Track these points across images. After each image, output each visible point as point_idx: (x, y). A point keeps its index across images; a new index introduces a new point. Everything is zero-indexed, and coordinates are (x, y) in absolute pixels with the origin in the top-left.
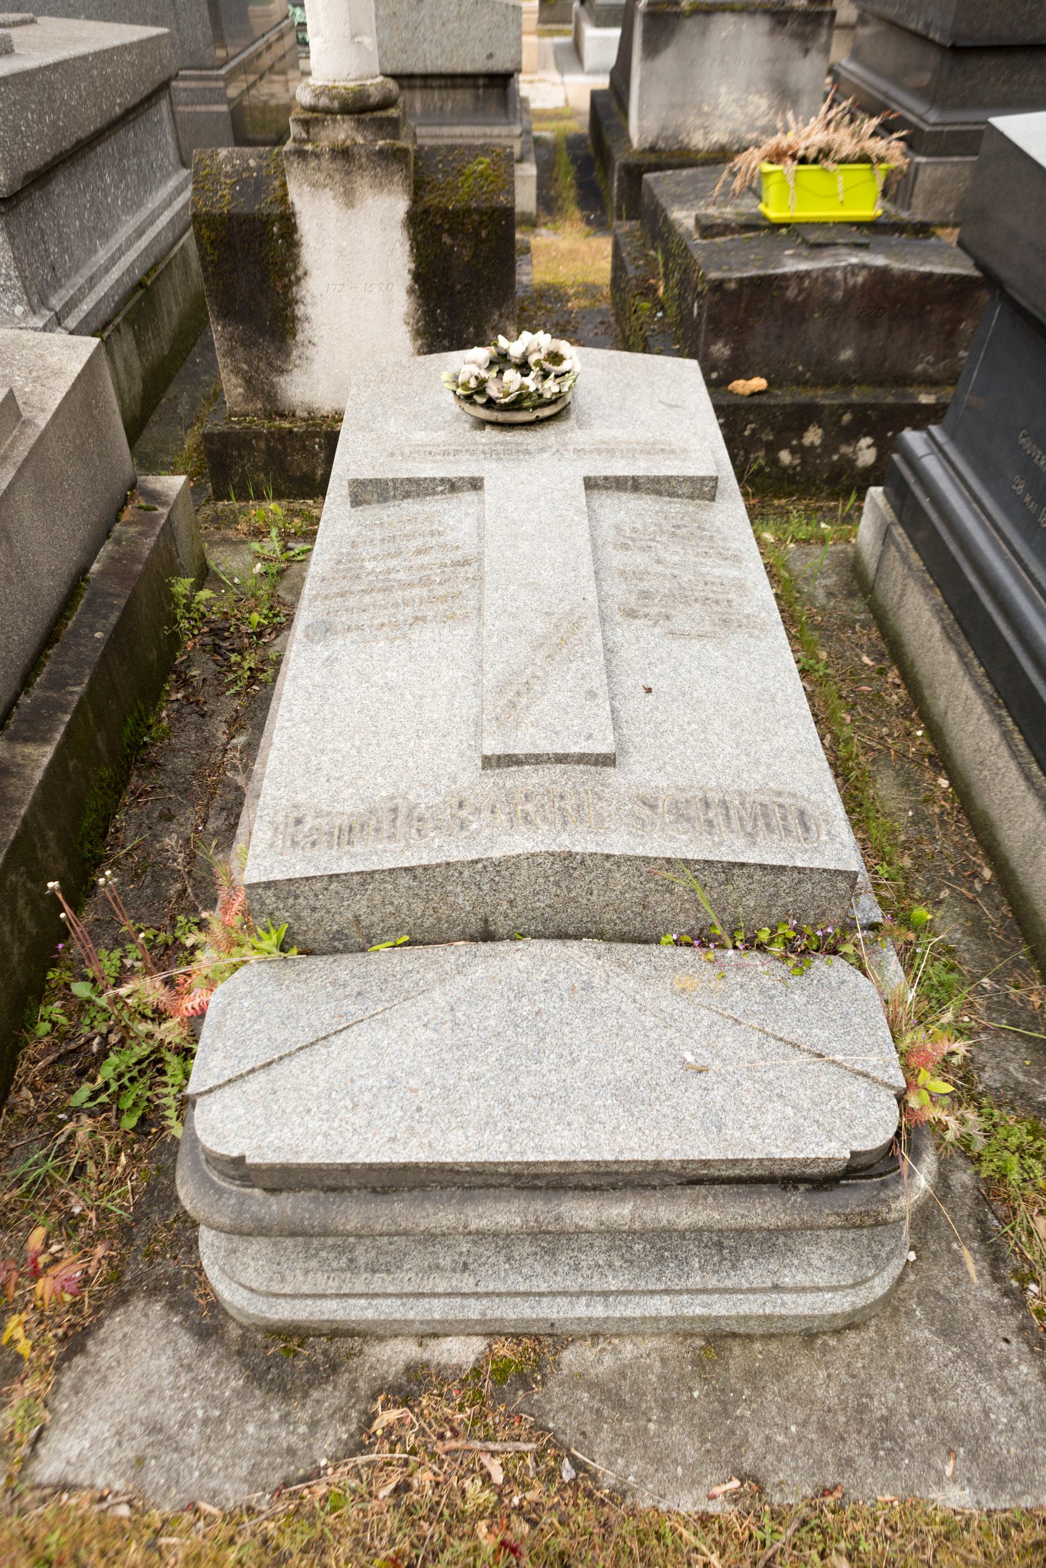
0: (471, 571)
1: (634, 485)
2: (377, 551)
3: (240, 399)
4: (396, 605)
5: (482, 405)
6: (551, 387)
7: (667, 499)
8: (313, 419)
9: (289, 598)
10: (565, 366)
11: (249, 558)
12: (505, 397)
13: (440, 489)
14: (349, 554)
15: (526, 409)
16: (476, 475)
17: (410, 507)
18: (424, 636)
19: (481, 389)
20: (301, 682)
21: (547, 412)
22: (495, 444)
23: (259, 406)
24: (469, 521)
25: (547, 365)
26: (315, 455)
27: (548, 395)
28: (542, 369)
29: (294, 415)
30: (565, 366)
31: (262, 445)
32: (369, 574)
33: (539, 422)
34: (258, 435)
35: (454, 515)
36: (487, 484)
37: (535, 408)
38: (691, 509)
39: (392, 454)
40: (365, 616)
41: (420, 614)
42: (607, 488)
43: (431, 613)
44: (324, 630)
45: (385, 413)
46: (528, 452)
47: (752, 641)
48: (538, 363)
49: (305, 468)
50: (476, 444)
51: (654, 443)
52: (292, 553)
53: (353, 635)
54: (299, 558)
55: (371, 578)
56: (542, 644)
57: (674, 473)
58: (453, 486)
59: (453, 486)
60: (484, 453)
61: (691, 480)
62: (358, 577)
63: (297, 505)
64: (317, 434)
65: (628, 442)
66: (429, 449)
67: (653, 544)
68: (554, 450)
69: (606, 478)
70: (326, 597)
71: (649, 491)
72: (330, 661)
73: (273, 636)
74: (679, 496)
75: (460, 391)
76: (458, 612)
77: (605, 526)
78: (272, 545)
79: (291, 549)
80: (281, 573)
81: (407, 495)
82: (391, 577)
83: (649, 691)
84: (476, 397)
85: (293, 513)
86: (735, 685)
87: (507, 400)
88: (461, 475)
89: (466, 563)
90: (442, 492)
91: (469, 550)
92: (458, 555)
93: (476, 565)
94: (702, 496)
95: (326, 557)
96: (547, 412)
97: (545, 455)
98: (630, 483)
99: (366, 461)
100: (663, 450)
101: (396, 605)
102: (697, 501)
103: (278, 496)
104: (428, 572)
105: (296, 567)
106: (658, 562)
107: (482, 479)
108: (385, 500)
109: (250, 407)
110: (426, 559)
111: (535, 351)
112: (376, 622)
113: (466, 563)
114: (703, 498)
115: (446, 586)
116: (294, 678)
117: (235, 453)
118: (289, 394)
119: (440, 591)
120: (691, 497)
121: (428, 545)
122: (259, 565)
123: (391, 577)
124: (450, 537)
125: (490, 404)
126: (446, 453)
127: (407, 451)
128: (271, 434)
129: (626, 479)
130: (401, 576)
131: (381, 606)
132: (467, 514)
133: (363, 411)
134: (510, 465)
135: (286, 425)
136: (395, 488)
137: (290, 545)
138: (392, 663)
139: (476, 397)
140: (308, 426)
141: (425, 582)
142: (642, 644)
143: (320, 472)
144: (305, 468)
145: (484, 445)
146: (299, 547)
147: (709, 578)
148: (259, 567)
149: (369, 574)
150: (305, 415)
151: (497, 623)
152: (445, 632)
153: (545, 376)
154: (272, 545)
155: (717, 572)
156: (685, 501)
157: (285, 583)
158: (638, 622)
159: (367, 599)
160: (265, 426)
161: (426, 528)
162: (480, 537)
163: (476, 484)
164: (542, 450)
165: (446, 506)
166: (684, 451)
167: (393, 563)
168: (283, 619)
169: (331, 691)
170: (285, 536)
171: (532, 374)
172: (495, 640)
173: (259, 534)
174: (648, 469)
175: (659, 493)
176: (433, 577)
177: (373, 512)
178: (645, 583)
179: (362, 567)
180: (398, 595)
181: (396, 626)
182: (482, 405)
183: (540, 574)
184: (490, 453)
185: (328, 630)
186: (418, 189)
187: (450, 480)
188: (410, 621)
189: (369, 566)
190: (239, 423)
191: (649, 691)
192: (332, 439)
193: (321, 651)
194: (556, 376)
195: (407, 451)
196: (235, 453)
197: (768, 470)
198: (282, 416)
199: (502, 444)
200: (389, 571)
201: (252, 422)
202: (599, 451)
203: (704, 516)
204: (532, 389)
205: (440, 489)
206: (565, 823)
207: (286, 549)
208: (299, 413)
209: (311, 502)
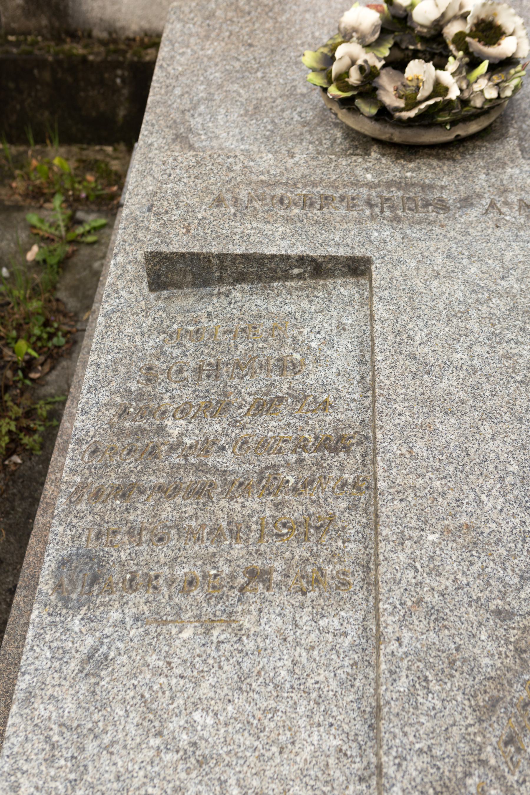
0: (347, 466)
2: (188, 395)
3: (19, 12)
4: (216, 533)
5: (371, 118)
6: (484, 88)
8: (115, 41)
9: (72, 304)
10: (506, 47)
11: (23, 236)
12: (408, 108)
13: (296, 271)
14: (140, 396)
15: (442, 125)
16: (358, 253)
17: (246, 301)
18: (268, 617)
19: (368, 88)
20: (41, 709)
21: (474, 128)
22: (389, 184)
23: (44, 22)
24: (345, 344)
25: (475, 45)
26: (116, 90)
27: (478, 103)
28: (467, 53)
29: (90, 36)
30: (506, 47)
31: (47, 76)
32: (172, 448)
33: (460, 142)
34: (42, 64)
35: (320, 325)
36: (378, 272)
37: (454, 123)
39: (219, 202)
40: (163, 553)
41: (259, 564)
43: (278, 565)
44: (88, 577)
45: (210, 99)
46: (442, 206)
48: (460, 38)
49: (102, 106)
50: (356, 184)
52: (80, 230)
53: (138, 600)
54: (90, 239)
55: (176, 460)
56: (494, 702)
58: (317, 269)
59: (317, 269)
60: (370, 204)
62: (153, 453)
63: (93, 153)
64: (119, 65)
66: (279, 191)
68: (486, 202)
70: (97, 495)
72: (95, 662)
73: (47, 368)
75: (333, 91)
76: (328, 569)
78: (56, 209)
79: (80, 222)
80: (64, 264)
81: (241, 278)
82: (211, 460)
84: (359, 103)
85: (86, 166)
87: (412, 114)
88: (332, 251)
89: (337, 444)
90: (299, 277)
91: (347, 414)
92: (324, 424)
93: (358, 451)
95: (104, 397)
96: (474, 128)
97: (473, 214)
99: (176, 215)
101: (216, 533)
103: (67, 139)
104: (273, 459)
105: (85, 251)
107: (367, 261)
108: (205, 283)
109: (32, 24)
110: (271, 426)
111: (455, 17)
112: (180, 572)
113: (337, 444)
115: (309, 495)
116: (29, 699)
117: (11, 85)
118: (84, 8)
119: (296, 510)
121: (276, 392)
122: (35, 249)
123: (211, 460)
124: (314, 377)
125: (384, 114)
126: (307, 203)
127: (243, 194)
128: (59, 62)
130: (226, 461)
131: (191, 531)
132: (341, 328)
133: (178, 91)
134: (413, 233)
135: (79, 50)
136: (222, 268)
137: (80, 215)
138: (205, 689)
139: (359, 103)
140: (108, 52)
141: (267, 482)
143: (122, 113)
144: (102, 106)
145: (371, 186)
146: (93, 220)
148: (33, 254)
149: (172, 448)
150: (104, 35)
151: (406, 635)
152: (304, 618)
153: (473, 62)
154: (56, 209)
157: (69, 279)
159: (167, 511)
160: (49, 51)
161: (271, 352)
162: (370, 387)
163: (357, 268)
164: (466, 202)
165: (305, 304)
167: (215, 427)
168: (63, 340)
169: (91, 747)
170: (73, 202)
171: (452, 65)
172: (403, 684)
173: (39, 196)
176: (283, 473)
177: (189, 306)
179: (161, 430)
180: (222, 509)
181: (215, 588)
182: (371, 118)
183: (479, 503)
184: (382, 207)
185: (95, 579)
186: (406, 99)
187: (313, 260)
188: (241, 580)
189: (175, 428)
190: (17, 44)
192: (141, 76)
193: (80, 634)
194: (493, 68)
195: (243, 194)
196: (11, 85)
198: (73, 36)
199: (398, 185)
200: (207, 446)
201: (34, 43)
204: (454, 94)
205: (296, 271)
207: (74, 222)
208: (97, 33)
209: (109, 149)
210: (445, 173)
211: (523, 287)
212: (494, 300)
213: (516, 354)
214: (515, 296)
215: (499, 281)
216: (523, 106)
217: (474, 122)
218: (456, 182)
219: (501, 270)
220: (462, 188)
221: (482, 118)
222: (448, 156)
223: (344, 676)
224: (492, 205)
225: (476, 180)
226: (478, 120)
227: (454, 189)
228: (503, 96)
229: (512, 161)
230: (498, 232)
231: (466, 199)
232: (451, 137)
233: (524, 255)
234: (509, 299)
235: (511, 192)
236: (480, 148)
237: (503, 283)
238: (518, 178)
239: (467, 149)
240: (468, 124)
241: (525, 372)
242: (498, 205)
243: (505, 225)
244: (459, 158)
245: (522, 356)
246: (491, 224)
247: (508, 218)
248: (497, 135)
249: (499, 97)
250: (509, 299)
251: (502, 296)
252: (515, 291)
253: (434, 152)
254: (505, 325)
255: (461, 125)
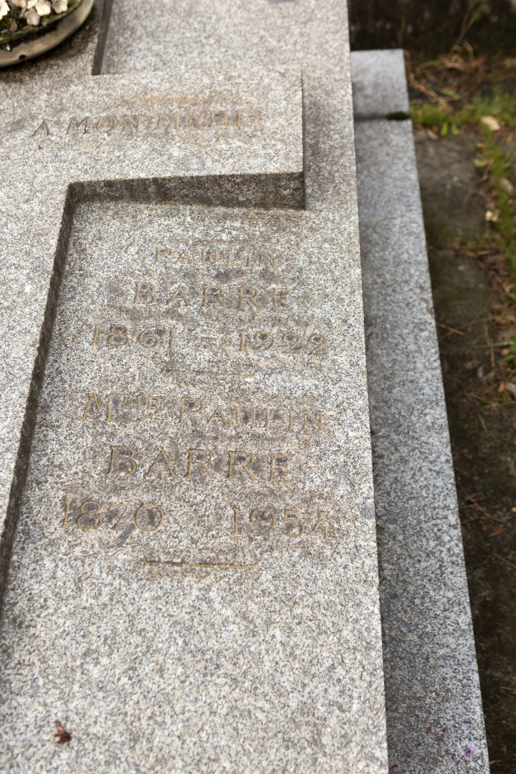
1: (160, 191)
7: (221, 210)
21: (39, 46)
37: (14, 43)
38: (260, 228)
42: (116, 199)
47: (305, 567)
51: (208, 102)
57: (226, 171)
61: (256, 179)
65: (166, 101)
67: (168, 323)
69: (109, 184)
71: (186, 200)
74: (240, 204)
77: (92, 285)
83: (65, 737)
86: (248, 701)
94: (281, 202)
96: (39, 46)
97: (21, 136)
98: (152, 189)
100: (220, 115)
102: (273, 211)
106: (168, 369)
114: (283, 206)
120: (263, 204)
129: (143, 183)
142: (86, 599)
147: (256, 403)
155: (274, 384)
156: (253, 212)
158: (92, 535)
166: (257, 115)
174: (182, 162)
175: (207, 202)
178: (130, 429)
191: (65, 737)
197: (494, 19)
202: (111, 122)
203: (280, 244)
206: (294, 516)
210: (7, 96)
211: (44, 209)
212: (9, 226)
213: (12, 280)
214: (31, 220)
215: (21, 205)
216: (128, 18)
217: (38, 41)
218: (16, 105)
219: (28, 193)
220: (19, 110)
221: (48, 36)
222: (17, 78)
223: (110, 577)
224: (44, 126)
225: (36, 101)
226: (43, 38)
227: (11, 112)
228: (58, 11)
229: (79, 78)
230: (39, 154)
231: (18, 122)
232: (15, 58)
233: (56, 176)
234: (25, 223)
235: (67, 110)
236: (52, 66)
237: (25, 207)
238: (78, 96)
239: (39, 69)
240: (31, 43)
241: (15, 297)
242: (49, 126)
243: (48, 145)
244: (27, 78)
245: (17, 281)
246: (35, 146)
247: (53, 138)
248: (72, 52)
249: (53, 12)
250: (25, 223)
251: (19, 220)
252: (34, 214)
253: (4, 76)
254: (12, 250)
255: (23, 45)
